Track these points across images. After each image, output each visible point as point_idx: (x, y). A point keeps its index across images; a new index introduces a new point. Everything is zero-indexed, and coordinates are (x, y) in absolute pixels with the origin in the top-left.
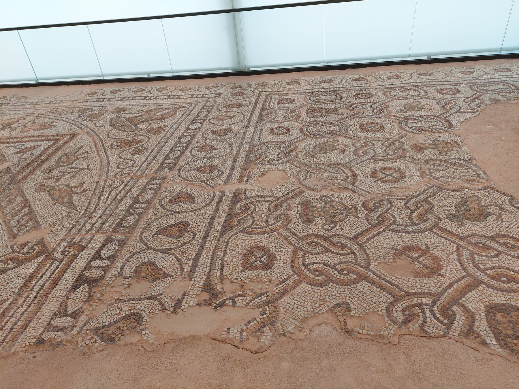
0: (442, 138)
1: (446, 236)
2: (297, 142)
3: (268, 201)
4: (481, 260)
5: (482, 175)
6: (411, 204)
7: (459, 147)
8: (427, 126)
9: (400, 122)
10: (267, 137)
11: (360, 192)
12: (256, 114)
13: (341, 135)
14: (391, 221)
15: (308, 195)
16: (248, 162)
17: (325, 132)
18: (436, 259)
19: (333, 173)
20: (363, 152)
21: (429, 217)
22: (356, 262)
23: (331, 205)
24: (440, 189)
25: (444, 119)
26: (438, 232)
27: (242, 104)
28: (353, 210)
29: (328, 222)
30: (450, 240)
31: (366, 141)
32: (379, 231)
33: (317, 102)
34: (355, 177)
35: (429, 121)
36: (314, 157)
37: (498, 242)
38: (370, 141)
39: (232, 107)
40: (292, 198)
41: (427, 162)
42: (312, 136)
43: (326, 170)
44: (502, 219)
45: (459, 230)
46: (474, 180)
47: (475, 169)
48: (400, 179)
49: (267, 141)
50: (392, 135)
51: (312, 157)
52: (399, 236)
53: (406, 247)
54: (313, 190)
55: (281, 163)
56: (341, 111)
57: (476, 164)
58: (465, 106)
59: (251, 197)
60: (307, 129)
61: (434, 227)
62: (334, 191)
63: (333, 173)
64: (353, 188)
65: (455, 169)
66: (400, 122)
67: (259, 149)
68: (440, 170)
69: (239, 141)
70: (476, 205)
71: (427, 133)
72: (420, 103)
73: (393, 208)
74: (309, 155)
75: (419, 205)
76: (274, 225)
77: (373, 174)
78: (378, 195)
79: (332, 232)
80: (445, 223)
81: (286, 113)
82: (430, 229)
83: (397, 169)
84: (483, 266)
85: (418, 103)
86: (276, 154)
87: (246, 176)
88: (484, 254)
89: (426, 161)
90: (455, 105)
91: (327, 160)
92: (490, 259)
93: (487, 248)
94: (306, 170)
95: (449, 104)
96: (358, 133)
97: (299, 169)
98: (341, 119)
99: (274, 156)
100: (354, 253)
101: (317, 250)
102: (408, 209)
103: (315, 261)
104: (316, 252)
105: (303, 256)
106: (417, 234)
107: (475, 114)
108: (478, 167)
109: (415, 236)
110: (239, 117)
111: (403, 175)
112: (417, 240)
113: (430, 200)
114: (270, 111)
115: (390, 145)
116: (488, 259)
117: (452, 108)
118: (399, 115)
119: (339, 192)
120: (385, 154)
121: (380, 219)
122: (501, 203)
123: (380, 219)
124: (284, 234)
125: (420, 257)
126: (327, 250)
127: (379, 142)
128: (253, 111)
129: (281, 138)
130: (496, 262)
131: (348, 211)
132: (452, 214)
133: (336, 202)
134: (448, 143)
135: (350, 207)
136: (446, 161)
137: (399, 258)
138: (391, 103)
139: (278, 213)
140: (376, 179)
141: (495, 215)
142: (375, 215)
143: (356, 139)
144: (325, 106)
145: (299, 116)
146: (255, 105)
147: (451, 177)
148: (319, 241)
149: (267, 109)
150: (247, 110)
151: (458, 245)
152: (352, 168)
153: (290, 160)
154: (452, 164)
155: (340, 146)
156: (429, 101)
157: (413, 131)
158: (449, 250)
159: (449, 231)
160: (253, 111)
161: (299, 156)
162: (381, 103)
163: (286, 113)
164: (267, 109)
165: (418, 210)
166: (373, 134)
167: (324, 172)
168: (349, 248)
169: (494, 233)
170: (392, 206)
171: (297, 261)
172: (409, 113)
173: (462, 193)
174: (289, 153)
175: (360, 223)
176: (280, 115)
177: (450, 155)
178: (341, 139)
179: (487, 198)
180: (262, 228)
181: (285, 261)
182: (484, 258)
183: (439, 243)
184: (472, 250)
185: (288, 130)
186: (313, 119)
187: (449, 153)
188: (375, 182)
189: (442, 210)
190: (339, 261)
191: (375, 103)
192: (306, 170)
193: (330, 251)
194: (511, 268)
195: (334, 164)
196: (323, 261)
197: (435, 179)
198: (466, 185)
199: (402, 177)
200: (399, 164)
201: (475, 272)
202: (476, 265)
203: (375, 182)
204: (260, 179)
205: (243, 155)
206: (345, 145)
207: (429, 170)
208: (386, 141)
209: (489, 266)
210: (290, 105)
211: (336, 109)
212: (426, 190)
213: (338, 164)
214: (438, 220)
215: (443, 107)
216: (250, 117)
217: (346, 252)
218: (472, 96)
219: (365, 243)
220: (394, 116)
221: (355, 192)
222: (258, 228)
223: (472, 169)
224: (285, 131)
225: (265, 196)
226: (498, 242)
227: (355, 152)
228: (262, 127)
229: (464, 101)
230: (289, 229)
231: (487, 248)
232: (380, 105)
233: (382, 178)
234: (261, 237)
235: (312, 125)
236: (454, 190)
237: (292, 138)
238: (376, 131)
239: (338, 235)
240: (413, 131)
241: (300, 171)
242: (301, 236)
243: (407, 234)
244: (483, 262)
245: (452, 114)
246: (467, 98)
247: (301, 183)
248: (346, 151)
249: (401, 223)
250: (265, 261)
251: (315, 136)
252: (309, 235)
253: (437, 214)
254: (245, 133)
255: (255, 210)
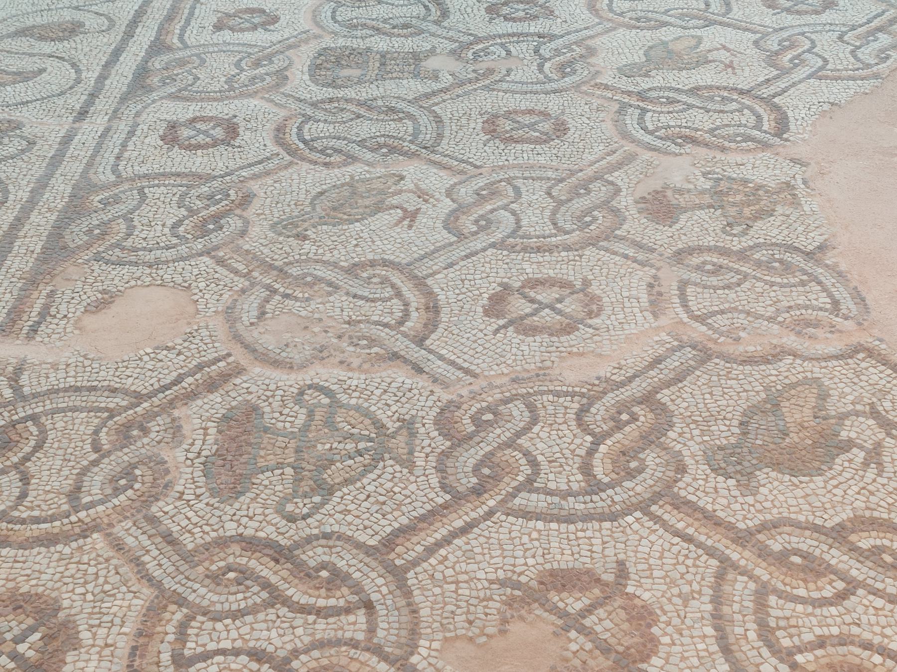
0: (746, 172)
1: (690, 531)
2: (255, 177)
3: (100, 410)
4: (788, 613)
5: (848, 304)
6: (599, 411)
7: (795, 202)
8: (708, 126)
9: (623, 108)
10: (148, 153)
11: (439, 368)
12: (128, 65)
13: (414, 155)
14: (521, 478)
15: (257, 381)
16: (56, 250)
17: (362, 143)
18: (642, 618)
19: (362, 298)
20: (476, 222)
21: (649, 462)
22: (370, 640)
23: (329, 423)
24: (705, 355)
25: (766, 101)
26: (666, 517)
27: (81, 25)
28: (401, 439)
29: (305, 487)
30: (699, 545)
31: (495, 177)
32: (473, 515)
33: (355, 27)
34: (431, 315)
35: (717, 107)
36: (305, 238)
37: (854, 549)
38: (509, 181)
39: (41, 38)
40: (191, 396)
41: (680, 256)
42: (314, 156)
43: (337, 288)
44: (880, 464)
45: (737, 506)
46: (817, 324)
47: (828, 281)
48: (581, 321)
49: (144, 170)
50: (588, 157)
51: (297, 236)
52: (535, 535)
53: (552, 573)
54: (276, 364)
55: (183, 259)
56: (431, 64)
57: (836, 265)
58: (840, 57)
59: (34, 396)
60: (300, 129)
61: (656, 498)
62: (349, 367)
63: (362, 298)
64: (417, 354)
65: (766, 282)
66: (623, 108)
67: (106, 203)
68: (715, 289)
69: (38, 170)
70: (808, 412)
71: (702, 151)
72: (700, 40)
73: (536, 429)
74: (291, 228)
75: (625, 417)
76: (100, 508)
77: (496, 305)
78: (498, 382)
79: (310, 527)
80: (703, 486)
81: (238, 65)
82: (644, 507)
83: (578, 284)
84: (791, 636)
85: (693, 42)
86: (169, 223)
87: (37, 308)
88: (802, 592)
89: (679, 253)
90: (809, 51)
91: (350, 247)
92: (818, 611)
93: (814, 568)
94: (268, 287)
95: (792, 47)
96: (476, 147)
97: (242, 283)
98: (427, 96)
99: (160, 232)
100: (369, 606)
101: (237, 601)
102: (587, 430)
103: (222, 645)
104: (234, 607)
105: (183, 627)
106: (596, 525)
107: (868, 85)
108: (840, 274)
109: (589, 533)
110: (58, 75)
111: (593, 306)
112: (587, 547)
113: (664, 396)
114: (180, 54)
115: (574, 193)
116: (810, 609)
117: (798, 62)
118: (624, 83)
119: (366, 372)
120: (549, 229)
121: (486, 471)
122: (887, 404)
123: (486, 471)
124: (130, 540)
125: (589, 610)
126: (276, 598)
127: (537, 184)
128: (116, 54)
129: (198, 162)
130: (833, 620)
131: (383, 444)
132: (721, 448)
133: (349, 407)
134: (759, 187)
135: (392, 426)
136: (743, 255)
137: (522, 618)
138: (605, 39)
139: (125, 456)
140: (501, 322)
141: (861, 448)
142: (470, 457)
143: (462, 169)
144: (381, 44)
145: (282, 77)
146: (129, 34)
147: (748, 313)
148: (253, 563)
149: (170, 49)
150: (91, 50)
151: (724, 560)
152: (429, 281)
153: (217, 248)
154: (759, 264)
155: (404, 196)
156: (728, 36)
157: (659, 143)
158: (690, 583)
159: (703, 510)
160: (116, 54)
161: (255, 231)
162: (573, 38)
163: (238, 65)
164: (170, 49)
165: (618, 436)
166: (522, 154)
167: (330, 294)
168: (357, 588)
169: (845, 514)
170: (534, 421)
171: (153, 648)
172: (658, 79)
173: (770, 369)
174: (217, 218)
175: (413, 487)
176: (219, 68)
177: (769, 230)
178: (412, 170)
179: (847, 388)
180: (52, 519)
181: (107, 652)
182: (800, 608)
183: (661, 558)
184: (766, 577)
185: (232, 130)
186: (330, 92)
187: (759, 223)
188: (496, 331)
189: (696, 432)
190: (307, 640)
191: (552, 37)
192: (268, 287)
193: (286, 602)
194: (877, 640)
195: (372, 264)
196: (251, 644)
197: (696, 318)
198: (790, 340)
199: (590, 315)
200: (589, 266)
201: (759, 660)
202: (766, 634)
203: (496, 331)
204: (90, 321)
205: (42, 221)
206: (423, 195)
207: (683, 285)
208: (562, 180)
209: (808, 637)
210: (260, 37)
211: (417, 57)
212: (658, 361)
213: (385, 263)
214: (677, 471)
215: (772, 59)
216: (102, 78)
217: (342, 602)
218: (869, 21)
219: (415, 563)
220: (607, 87)
221: (419, 370)
222: (37, 520)
223: (819, 283)
224: (219, 133)
225: (94, 389)
226: (854, 549)
227: (451, 223)
228: (138, 114)
229: (841, 38)
230: (153, 520)
231: (814, 568)
232: (569, 47)
233: (522, 318)
234: (39, 556)
235: (320, 115)
236: (749, 360)
237: (240, 163)
238: (537, 141)
239: (326, 536)
240: (659, 143)
241: (243, 291)
242: (190, 546)
243: (563, 526)
244: (793, 622)
245: (794, 85)
246: (853, 28)
247: (237, 338)
248: (420, 216)
249: (552, 486)
250: (31, 653)
251: (324, 154)
252: (222, 543)
253: (678, 447)
254: (67, 140)
255: (38, 447)
